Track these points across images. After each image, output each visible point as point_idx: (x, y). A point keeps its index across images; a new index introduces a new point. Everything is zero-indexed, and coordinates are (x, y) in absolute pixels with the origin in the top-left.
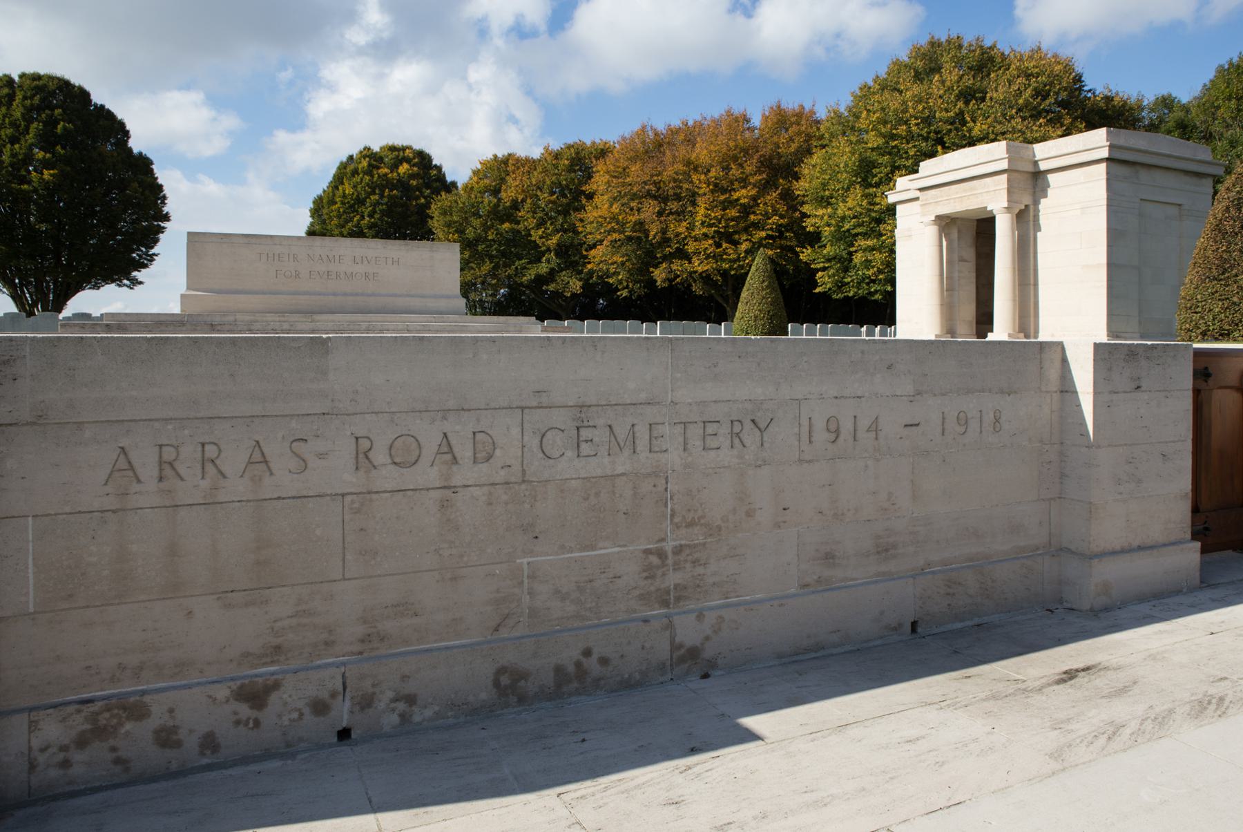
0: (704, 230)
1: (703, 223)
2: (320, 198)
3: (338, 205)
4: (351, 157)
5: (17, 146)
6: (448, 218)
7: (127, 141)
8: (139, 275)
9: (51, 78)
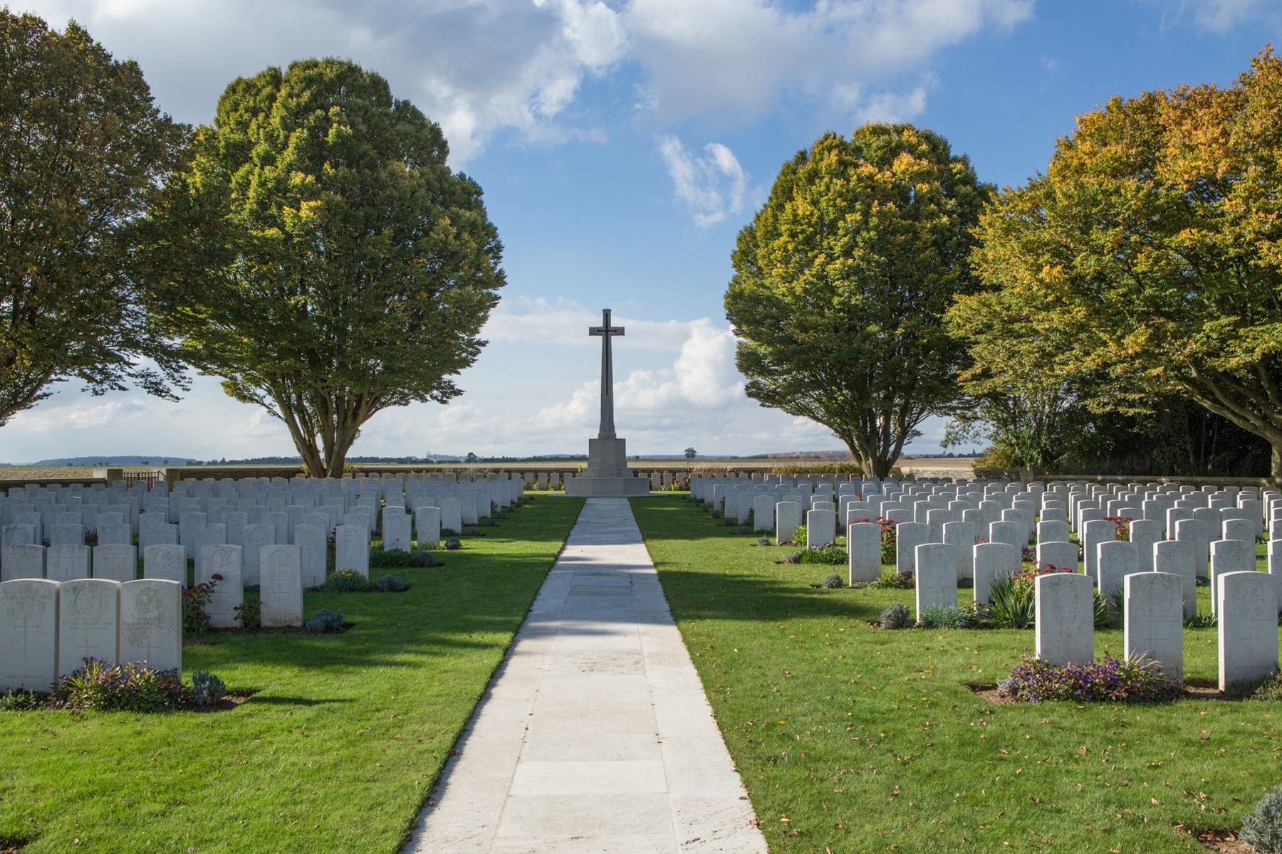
2: (751, 232)
3: (785, 238)
8: (457, 380)
9: (329, 63)
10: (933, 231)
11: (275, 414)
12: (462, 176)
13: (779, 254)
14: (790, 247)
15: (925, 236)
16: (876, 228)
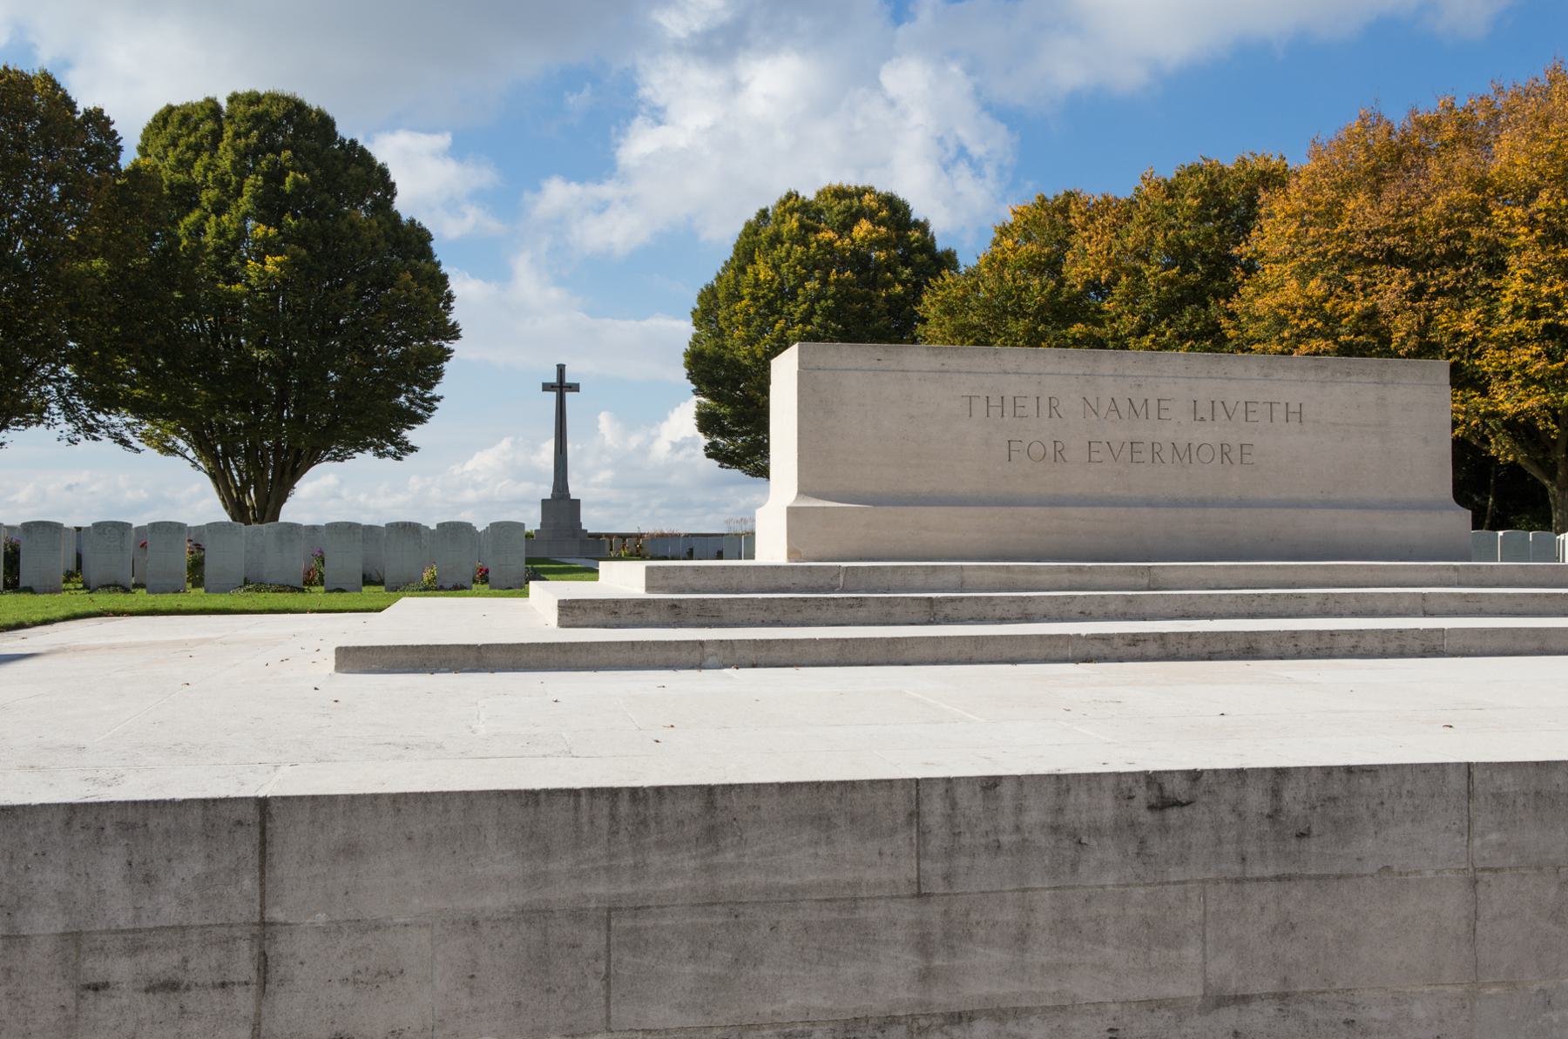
0: (1520, 324)
1: (1517, 308)
4: (763, 214)
5: (225, 218)
6: (960, 320)
7: (391, 201)
8: (412, 435)
9: (275, 98)
10: (888, 299)
11: (200, 469)
12: (412, 222)
13: (740, 317)
14: (752, 311)
15: (880, 304)
16: (833, 297)
